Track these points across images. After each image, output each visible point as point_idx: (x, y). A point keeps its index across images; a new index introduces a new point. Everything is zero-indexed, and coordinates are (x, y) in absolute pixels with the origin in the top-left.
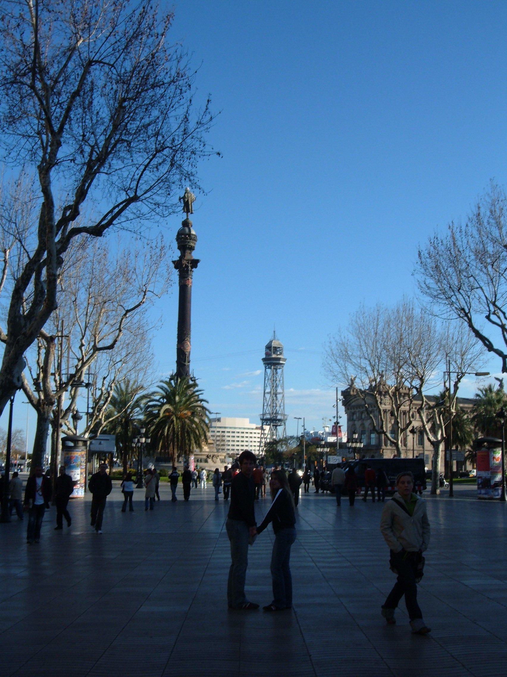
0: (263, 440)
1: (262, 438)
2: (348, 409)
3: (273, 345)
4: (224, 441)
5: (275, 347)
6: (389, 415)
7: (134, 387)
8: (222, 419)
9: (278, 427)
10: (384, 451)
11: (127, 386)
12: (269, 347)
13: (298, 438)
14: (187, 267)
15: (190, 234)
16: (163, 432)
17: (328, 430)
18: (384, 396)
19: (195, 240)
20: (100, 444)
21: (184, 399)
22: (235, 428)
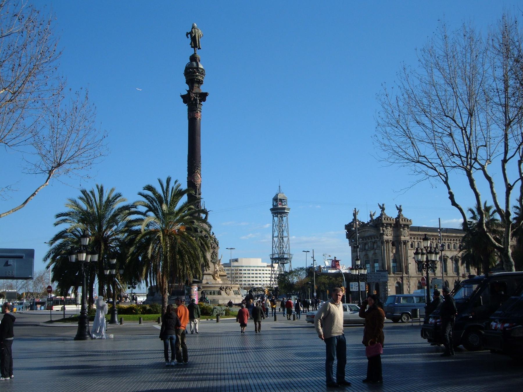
0: (273, 276)
1: (272, 274)
3: (279, 197)
5: (281, 199)
6: (390, 244)
9: (285, 265)
12: (275, 199)
15: (197, 68)
18: (386, 227)
20: (7, 264)
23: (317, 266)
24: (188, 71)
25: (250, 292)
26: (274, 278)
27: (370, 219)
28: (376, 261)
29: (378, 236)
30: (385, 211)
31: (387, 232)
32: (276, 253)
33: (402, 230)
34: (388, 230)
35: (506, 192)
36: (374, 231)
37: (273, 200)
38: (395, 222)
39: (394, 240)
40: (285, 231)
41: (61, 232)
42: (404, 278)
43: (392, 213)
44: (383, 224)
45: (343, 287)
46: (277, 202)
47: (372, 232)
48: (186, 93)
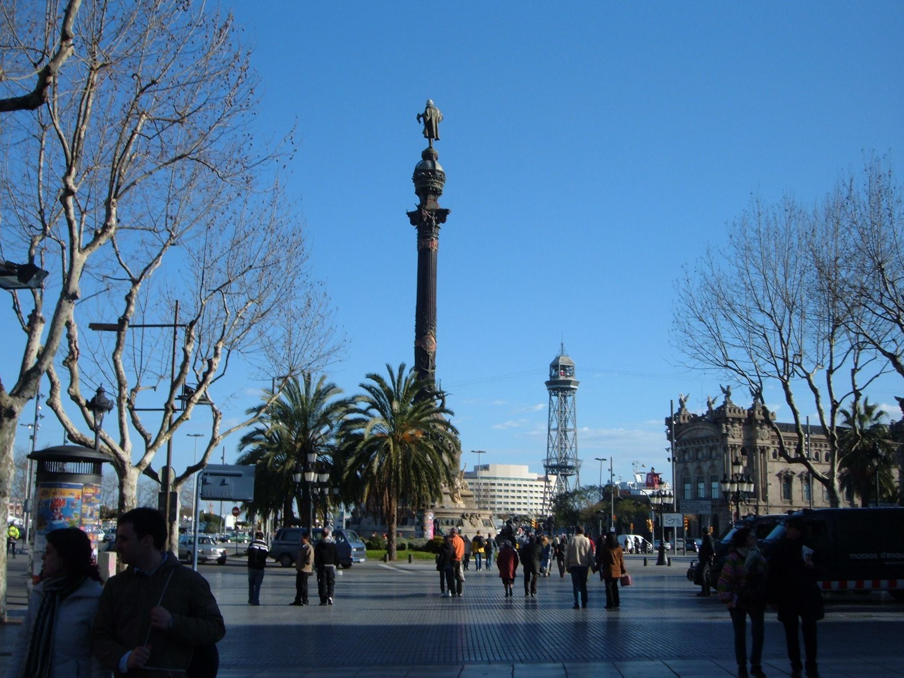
0: (548, 496)
1: (547, 493)
3: (561, 362)
5: (564, 366)
8: (490, 467)
9: (568, 478)
11: (308, 385)
12: (555, 366)
13: (601, 488)
14: (430, 221)
15: (434, 171)
16: (371, 467)
17: (639, 479)
18: (732, 424)
19: (442, 180)
20: (223, 483)
22: (509, 479)
24: (419, 174)
25: (509, 522)
27: (707, 409)
28: (699, 480)
30: (731, 398)
32: (554, 456)
33: (758, 428)
35: (831, 411)
40: (570, 421)
41: (250, 434)
42: (760, 508)
43: (742, 401)
44: (727, 418)
46: (556, 370)
47: (707, 431)
48: (415, 209)
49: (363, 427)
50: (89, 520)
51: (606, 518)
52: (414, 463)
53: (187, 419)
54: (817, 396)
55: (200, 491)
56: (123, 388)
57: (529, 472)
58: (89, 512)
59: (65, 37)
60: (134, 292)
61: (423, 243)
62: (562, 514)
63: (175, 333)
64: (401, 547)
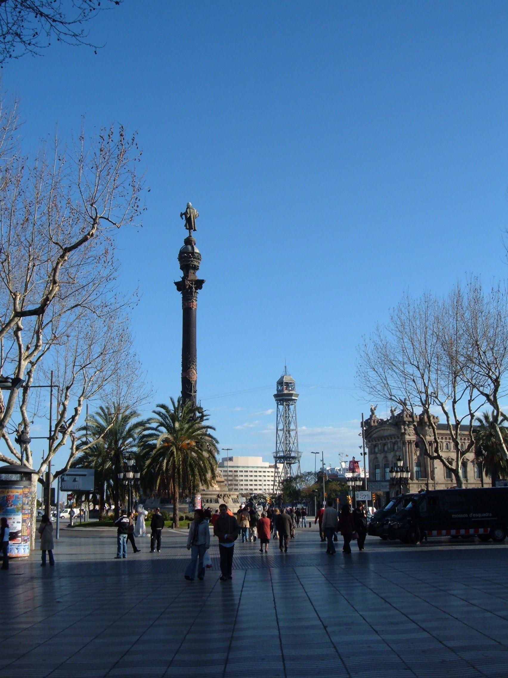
1: (276, 477)
2: (369, 441)
3: (285, 380)
4: (237, 480)
5: (287, 383)
7: (127, 413)
8: (234, 459)
9: (292, 465)
10: (410, 485)
12: (280, 383)
14: (191, 288)
15: (193, 253)
16: (161, 466)
17: (344, 465)
18: (408, 426)
19: (199, 259)
20: (75, 480)
21: (186, 426)
22: (248, 467)
23: (331, 467)
24: (183, 255)
26: (278, 482)
29: (399, 436)
31: (409, 431)
33: (427, 428)
34: (410, 428)
36: (394, 429)
37: (277, 384)
38: (418, 420)
39: (418, 441)
44: (405, 422)
45: (349, 496)
47: (392, 431)
49: (156, 440)
50: (26, 506)
51: (320, 495)
52: (190, 462)
53: (64, 444)
54: (448, 417)
55: (60, 486)
56: (27, 427)
57: (263, 461)
58: (27, 502)
59: (55, 282)
60: (33, 370)
61: (186, 304)
62: (288, 493)
63: (52, 391)
64: (181, 519)
